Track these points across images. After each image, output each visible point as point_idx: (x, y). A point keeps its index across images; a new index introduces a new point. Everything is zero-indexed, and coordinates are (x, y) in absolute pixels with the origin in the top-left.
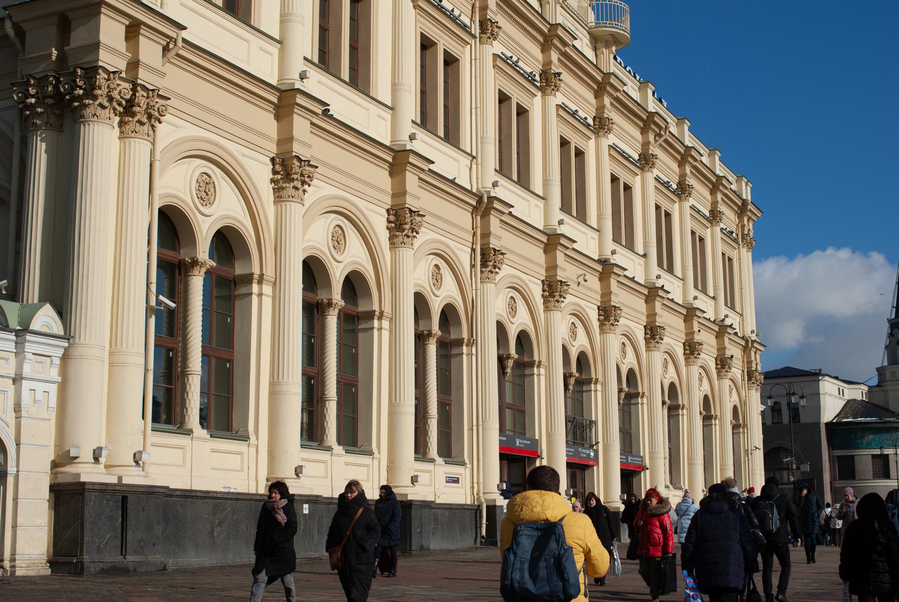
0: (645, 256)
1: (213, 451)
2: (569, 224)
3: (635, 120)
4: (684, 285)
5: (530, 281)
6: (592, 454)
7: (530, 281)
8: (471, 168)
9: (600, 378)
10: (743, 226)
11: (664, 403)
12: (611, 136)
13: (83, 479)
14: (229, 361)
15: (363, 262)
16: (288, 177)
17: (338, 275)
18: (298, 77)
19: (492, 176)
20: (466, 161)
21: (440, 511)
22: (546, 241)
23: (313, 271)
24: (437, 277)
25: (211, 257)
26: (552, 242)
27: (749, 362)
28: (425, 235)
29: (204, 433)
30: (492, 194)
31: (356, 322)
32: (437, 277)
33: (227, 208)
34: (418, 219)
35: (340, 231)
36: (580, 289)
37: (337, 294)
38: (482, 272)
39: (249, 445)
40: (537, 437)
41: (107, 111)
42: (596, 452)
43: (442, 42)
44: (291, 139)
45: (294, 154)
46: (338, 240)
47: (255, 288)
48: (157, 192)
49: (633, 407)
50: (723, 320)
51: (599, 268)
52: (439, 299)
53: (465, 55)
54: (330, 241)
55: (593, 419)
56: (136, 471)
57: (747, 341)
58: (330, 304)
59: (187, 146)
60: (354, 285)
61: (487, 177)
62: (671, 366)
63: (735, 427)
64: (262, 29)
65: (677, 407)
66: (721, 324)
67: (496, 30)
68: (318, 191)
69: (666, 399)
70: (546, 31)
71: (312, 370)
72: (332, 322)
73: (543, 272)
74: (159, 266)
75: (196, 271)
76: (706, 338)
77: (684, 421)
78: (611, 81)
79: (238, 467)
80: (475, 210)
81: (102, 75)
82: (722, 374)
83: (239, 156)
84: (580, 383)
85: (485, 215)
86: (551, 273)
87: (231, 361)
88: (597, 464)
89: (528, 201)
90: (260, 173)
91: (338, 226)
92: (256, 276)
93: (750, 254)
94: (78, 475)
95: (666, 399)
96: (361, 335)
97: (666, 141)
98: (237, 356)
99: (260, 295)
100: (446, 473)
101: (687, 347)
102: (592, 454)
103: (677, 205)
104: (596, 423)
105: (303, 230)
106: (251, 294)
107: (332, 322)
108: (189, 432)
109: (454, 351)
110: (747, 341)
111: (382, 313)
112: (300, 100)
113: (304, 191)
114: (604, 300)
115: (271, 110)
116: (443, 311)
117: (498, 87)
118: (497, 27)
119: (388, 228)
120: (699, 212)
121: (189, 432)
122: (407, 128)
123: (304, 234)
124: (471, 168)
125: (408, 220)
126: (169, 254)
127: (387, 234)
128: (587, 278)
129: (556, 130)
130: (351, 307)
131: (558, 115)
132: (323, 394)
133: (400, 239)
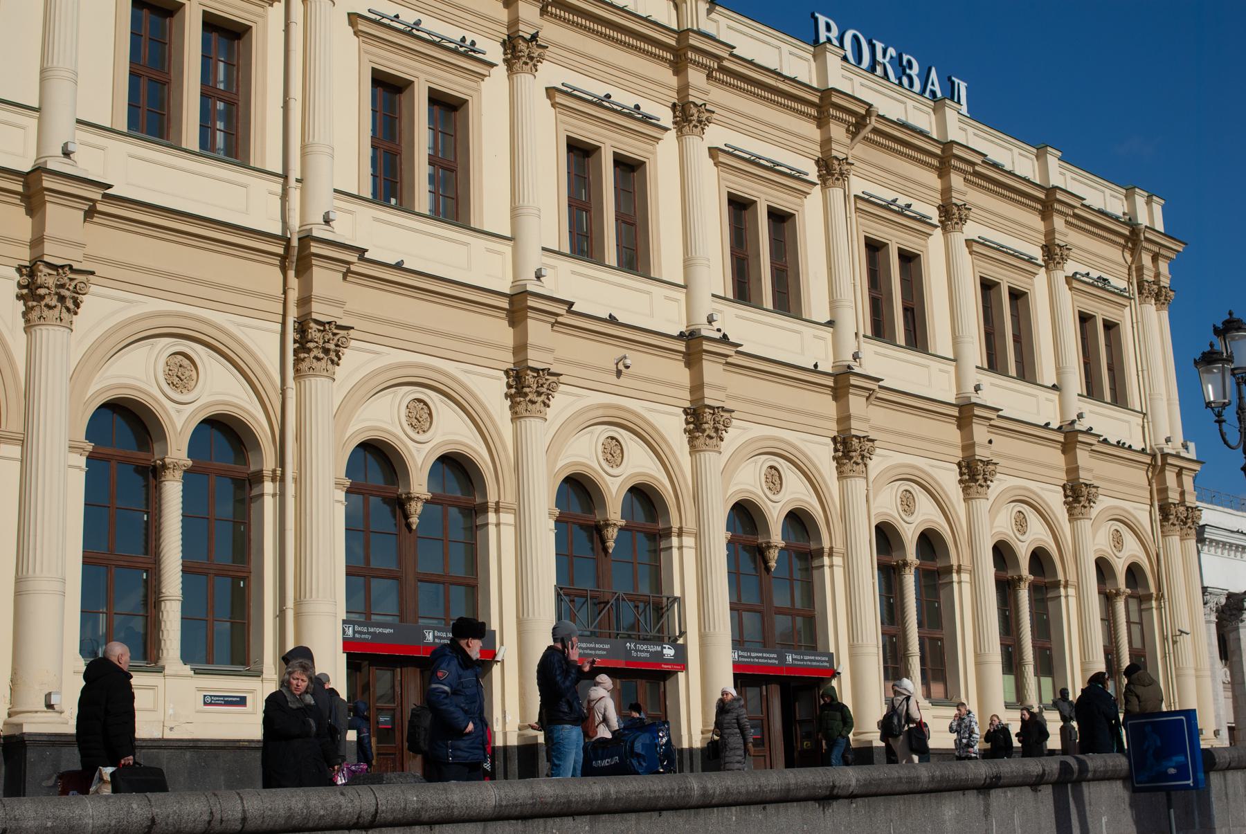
0: (830, 323)
3: (793, 104)
4: (957, 369)
8: (1143, 427)
10: (1140, 269)
12: (711, 130)
13: (27, 729)
14: (244, 579)
16: (973, 478)
18: (533, 277)
20: (1138, 420)
21: (166, 753)
22: (507, 306)
23: (1002, 553)
25: (1031, 573)
26: (1070, 438)
27: (1163, 491)
28: (1103, 503)
29: (187, 669)
30: (1166, 451)
32: (1118, 541)
33: (926, 514)
34: (1094, 490)
35: (186, 362)
36: (623, 380)
37: (1025, 570)
38: (1162, 526)
40: (832, 650)
41: (323, 362)
42: (682, 651)
43: (763, 197)
44: (1077, 469)
47: (826, 560)
48: (873, 513)
49: (815, 573)
50: (1073, 422)
51: (681, 346)
52: (1122, 561)
53: (1125, 318)
55: (677, 593)
56: (51, 715)
57: (1154, 456)
58: (769, 547)
59: (600, 412)
60: (1040, 559)
64: (486, 229)
66: (1069, 429)
67: (1066, 252)
68: (1000, 485)
70: (674, 43)
71: (893, 629)
72: (1024, 595)
73: (687, 395)
74: (879, 569)
75: (169, 474)
78: (691, 42)
79: (151, 706)
80: (1153, 465)
81: (855, 441)
82: (847, 468)
86: (521, 358)
87: (1050, 649)
88: (684, 667)
90: (672, 426)
91: (771, 467)
92: (955, 567)
93: (1165, 314)
94: (21, 725)
96: (1050, 604)
97: (875, 131)
98: (1054, 645)
99: (1067, 597)
100: (199, 689)
101: (1069, 492)
102: (669, 652)
104: (680, 601)
105: (990, 520)
106: (487, 524)
107: (1024, 595)
109: (816, 563)
110: (1154, 456)
111: (1067, 582)
112: (977, 411)
113: (988, 487)
114: (967, 454)
115: (18, 202)
117: (1076, 309)
118: (540, 46)
119: (834, 458)
123: (1094, 538)
124: (1143, 427)
125: (1173, 512)
126: (885, 558)
127: (685, 438)
128: (628, 362)
129: (968, 274)
130: (1039, 579)
132: (160, 592)
133: (702, 440)
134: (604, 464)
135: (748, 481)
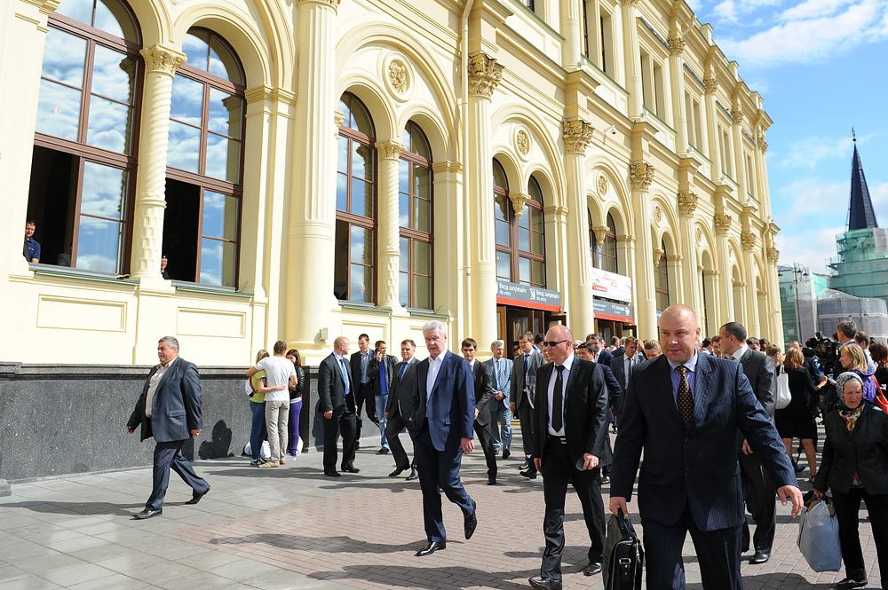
1: (183, 310)
2: (605, 86)
5: (618, 164)
6: (628, 312)
7: (618, 164)
9: (565, 208)
11: (699, 268)
15: (430, 107)
17: (604, 208)
19: (641, 110)
24: (602, 187)
29: (404, 312)
31: (426, 175)
39: (252, 305)
45: (644, 162)
46: (523, 146)
54: (388, 79)
61: (577, 60)
62: (703, 236)
63: (736, 285)
65: (711, 273)
69: (701, 265)
76: (704, 197)
77: (744, 296)
83: (543, 119)
84: (664, 258)
85: (473, 20)
89: (543, 36)
95: (701, 265)
97: (690, 32)
103: (667, 60)
108: (388, 312)
116: (609, 213)
120: (692, 74)
121: (388, 312)
122: (578, 58)
131: (638, 27)
134: (392, 88)
135: (370, 69)
